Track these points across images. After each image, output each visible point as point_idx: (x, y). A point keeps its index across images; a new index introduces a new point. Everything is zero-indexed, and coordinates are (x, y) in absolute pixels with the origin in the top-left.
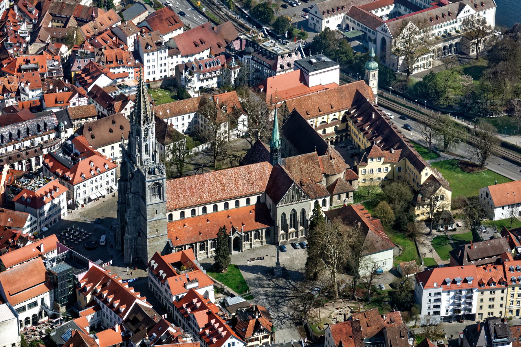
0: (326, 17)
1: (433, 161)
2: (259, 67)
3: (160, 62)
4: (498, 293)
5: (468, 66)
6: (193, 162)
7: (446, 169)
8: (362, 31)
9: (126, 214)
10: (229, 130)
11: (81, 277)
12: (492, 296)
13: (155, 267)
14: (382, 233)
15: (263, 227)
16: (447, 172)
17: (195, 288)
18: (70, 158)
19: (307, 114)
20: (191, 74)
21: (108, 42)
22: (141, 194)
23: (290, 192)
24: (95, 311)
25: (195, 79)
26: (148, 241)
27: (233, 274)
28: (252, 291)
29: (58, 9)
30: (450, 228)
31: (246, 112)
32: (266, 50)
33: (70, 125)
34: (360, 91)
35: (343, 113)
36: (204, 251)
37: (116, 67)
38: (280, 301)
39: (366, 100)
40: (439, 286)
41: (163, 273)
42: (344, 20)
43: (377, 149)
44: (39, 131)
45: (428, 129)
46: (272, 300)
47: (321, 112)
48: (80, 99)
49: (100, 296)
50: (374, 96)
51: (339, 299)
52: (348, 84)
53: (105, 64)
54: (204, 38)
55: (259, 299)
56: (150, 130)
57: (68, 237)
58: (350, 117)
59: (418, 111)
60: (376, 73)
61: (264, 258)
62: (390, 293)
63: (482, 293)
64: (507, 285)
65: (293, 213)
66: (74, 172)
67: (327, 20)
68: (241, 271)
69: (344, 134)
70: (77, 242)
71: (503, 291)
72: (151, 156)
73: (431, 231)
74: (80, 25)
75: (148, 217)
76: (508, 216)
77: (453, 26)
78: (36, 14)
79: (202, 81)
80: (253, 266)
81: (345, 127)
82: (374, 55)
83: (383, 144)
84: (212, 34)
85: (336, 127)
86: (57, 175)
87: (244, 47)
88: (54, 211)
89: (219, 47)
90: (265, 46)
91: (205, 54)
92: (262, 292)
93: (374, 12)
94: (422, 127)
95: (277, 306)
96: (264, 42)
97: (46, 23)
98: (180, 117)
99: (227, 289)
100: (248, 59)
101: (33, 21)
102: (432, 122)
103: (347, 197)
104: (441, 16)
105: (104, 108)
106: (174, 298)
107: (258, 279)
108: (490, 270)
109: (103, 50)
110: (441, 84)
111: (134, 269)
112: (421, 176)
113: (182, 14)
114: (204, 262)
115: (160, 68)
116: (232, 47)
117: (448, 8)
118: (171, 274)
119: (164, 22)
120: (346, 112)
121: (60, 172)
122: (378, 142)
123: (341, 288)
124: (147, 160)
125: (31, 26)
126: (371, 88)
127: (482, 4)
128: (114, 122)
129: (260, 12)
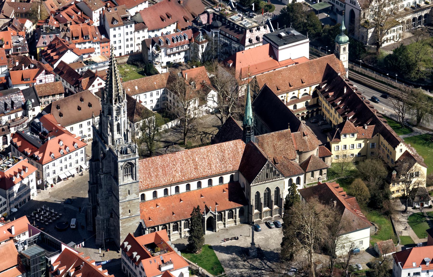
1: (406, 136)
2: (226, 41)
6: (163, 140)
7: (419, 144)
9: (98, 195)
10: (199, 106)
11: (53, 259)
14: (358, 212)
15: (237, 207)
19: (278, 90)
20: (158, 49)
21: (73, 17)
23: (264, 170)
25: (162, 54)
26: (120, 222)
27: (207, 255)
28: (228, 272)
30: (426, 206)
31: (216, 88)
32: (234, 24)
33: (38, 103)
34: (331, 65)
35: (313, 88)
36: (177, 232)
37: (82, 43)
39: (337, 74)
40: (418, 266)
43: (350, 124)
44: (6, 109)
45: (401, 103)
48: (46, 76)
50: (345, 70)
52: (318, 59)
53: (71, 39)
54: (171, 12)
56: (122, 109)
57: (38, 218)
58: (321, 92)
60: (347, 46)
61: (238, 238)
65: (267, 191)
66: (43, 151)
68: (216, 252)
69: (315, 110)
70: (47, 223)
72: (123, 135)
73: (406, 209)
75: (120, 198)
79: (169, 56)
80: (227, 246)
81: (316, 103)
83: (356, 119)
84: (178, 8)
85: (307, 102)
86: (26, 155)
87: (211, 21)
88: (23, 191)
89: (186, 21)
91: (171, 29)
94: (395, 101)
96: (232, 15)
98: (148, 94)
102: (404, 96)
103: (321, 174)
105: (70, 84)
107: (233, 260)
109: (69, 25)
110: (412, 55)
111: (107, 251)
115: (126, 43)
116: (199, 21)
118: (145, 256)
120: (316, 87)
121: (29, 152)
123: (317, 268)
124: (119, 139)
126: (342, 62)
128: (82, 100)
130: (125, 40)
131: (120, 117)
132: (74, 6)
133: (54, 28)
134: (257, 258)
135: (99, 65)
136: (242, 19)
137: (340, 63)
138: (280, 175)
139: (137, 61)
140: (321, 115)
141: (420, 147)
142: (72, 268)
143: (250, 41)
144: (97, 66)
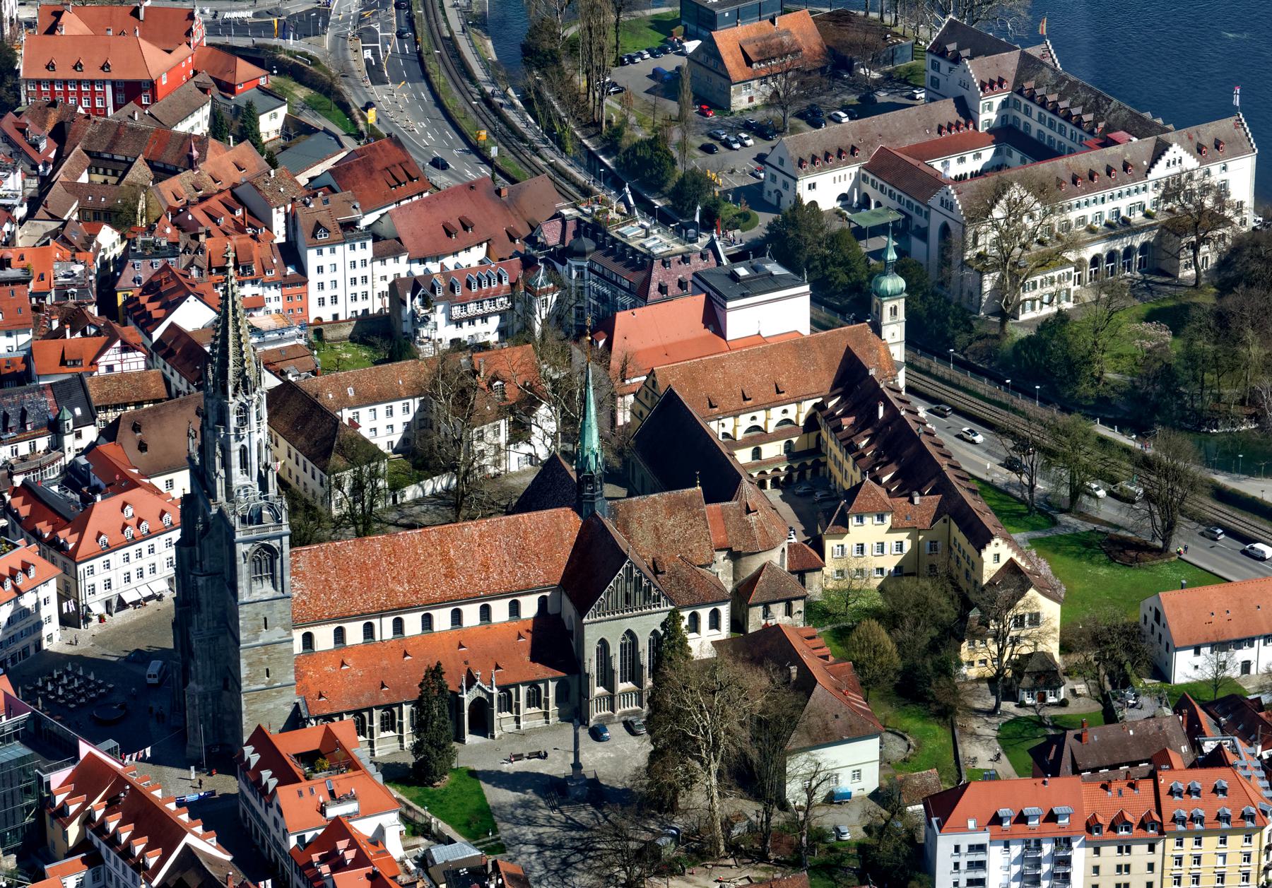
0: (807, 173)
1: (1038, 534)
2: (605, 290)
3: (352, 273)
4: (1140, 850)
5: (1171, 303)
6: (404, 521)
7: (1067, 554)
8: (899, 211)
9: (191, 629)
10: (508, 443)
11: (57, 778)
12: (1124, 859)
13: (253, 764)
16: (1068, 563)
17: (349, 816)
18: (77, 497)
19: (711, 406)
20: (426, 303)
21: (222, 221)
22: (227, 576)
23: (617, 584)
24: (86, 868)
25: (439, 316)
26: (243, 698)
27: (461, 791)
28: (505, 833)
29: (107, 139)
32: (625, 246)
33: (89, 419)
34: (857, 352)
35: (807, 406)
36: (391, 733)
38: (573, 859)
39: (867, 371)
40: (980, 828)
41: (271, 777)
42: (856, 184)
44: (6, 430)
46: (553, 857)
47: (749, 402)
48: (124, 355)
49: (101, 829)
51: (726, 858)
52: (824, 333)
53: (205, 273)
54: (472, 213)
55: (520, 853)
56: (253, 410)
57: (52, 693)
58: (826, 418)
59: (1014, 410)
60: (901, 304)
61: (546, 754)
62: (862, 848)
63: (1097, 851)
64: (1162, 832)
65: (629, 640)
66: (80, 526)
67: (811, 180)
69: (809, 462)
70: (72, 706)
71: (1152, 848)
72: (255, 478)
73: (998, 705)
74: (157, 180)
76: (1208, 673)
77: (1136, 198)
78: (48, 151)
79: (459, 323)
82: (895, 256)
83: (899, 481)
84: (494, 209)
86: (38, 537)
87: (569, 237)
88: (21, 626)
89: (512, 240)
90: (624, 236)
91: (473, 257)
92: (530, 836)
93: (937, 165)
95: (564, 871)
96: (623, 225)
97: (73, 174)
98: (381, 409)
99: (439, 825)
100: (578, 268)
101: (41, 167)
103: (789, 612)
104: (1103, 172)
105: (189, 382)
106: (293, 841)
107: (525, 805)
108: (1120, 792)
109: (202, 238)
110: (1081, 342)
111: (211, 775)
112: (982, 561)
113: (439, 164)
114: (392, 760)
116: (539, 239)
117: (1124, 153)
118: (287, 777)
119: (376, 175)
120: (815, 405)
121: (45, 529)
122: (885, 479)
123: (735, 832)
124: (244, 487)
125: (34, 183)
126: (887, 345)
127: (1217, 145)
129: (641, 159)
130: (348, 281)
131: (247, 432)
132: (228, 195)
133: (164, 243)
134: (585, 802)
135: (268, 336)
136: (647, 235)
137: (882, 347)
138: (662, 599)
139: (372, 333)
140: (824, 475)
141: (1049, 554)
142: (101, 801)
143: (663, 289)
144: (262, 340)
